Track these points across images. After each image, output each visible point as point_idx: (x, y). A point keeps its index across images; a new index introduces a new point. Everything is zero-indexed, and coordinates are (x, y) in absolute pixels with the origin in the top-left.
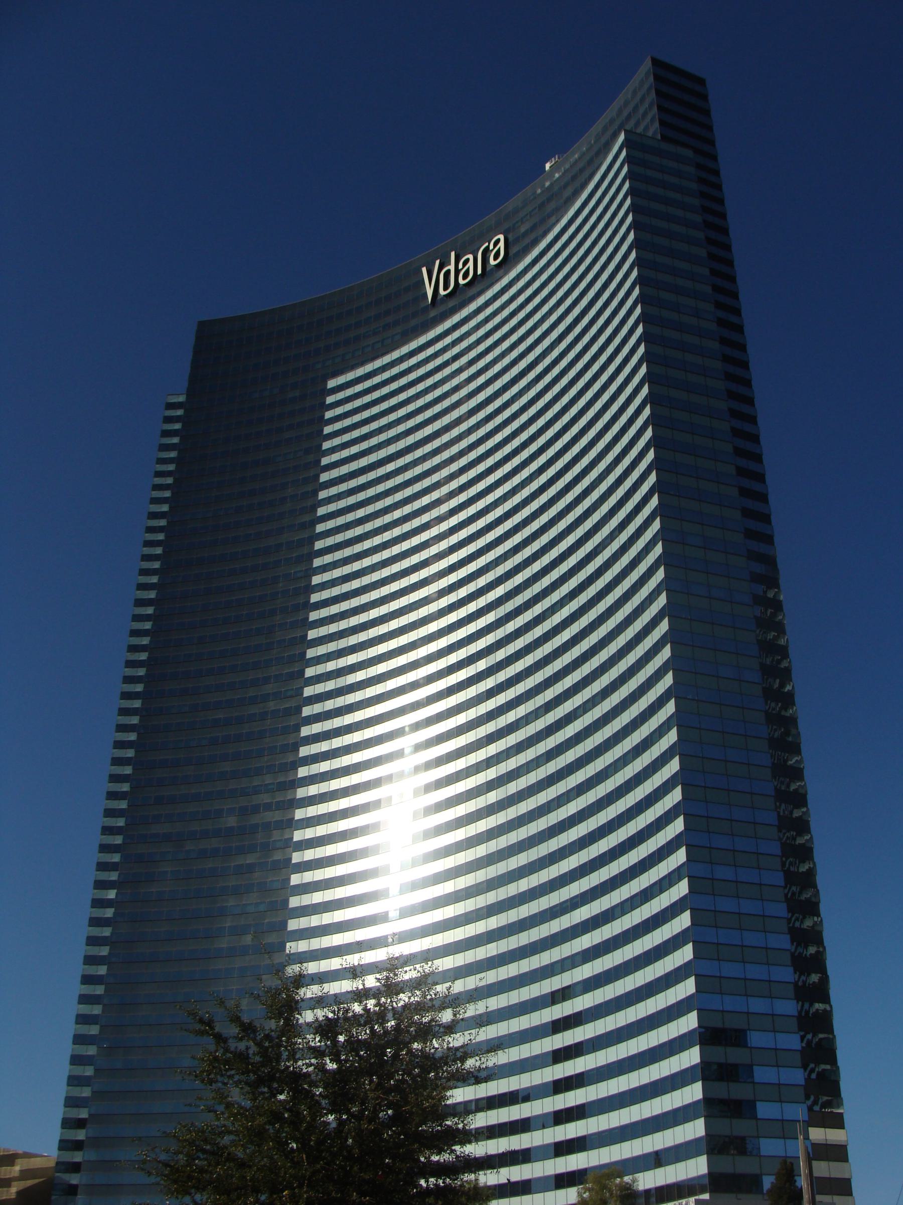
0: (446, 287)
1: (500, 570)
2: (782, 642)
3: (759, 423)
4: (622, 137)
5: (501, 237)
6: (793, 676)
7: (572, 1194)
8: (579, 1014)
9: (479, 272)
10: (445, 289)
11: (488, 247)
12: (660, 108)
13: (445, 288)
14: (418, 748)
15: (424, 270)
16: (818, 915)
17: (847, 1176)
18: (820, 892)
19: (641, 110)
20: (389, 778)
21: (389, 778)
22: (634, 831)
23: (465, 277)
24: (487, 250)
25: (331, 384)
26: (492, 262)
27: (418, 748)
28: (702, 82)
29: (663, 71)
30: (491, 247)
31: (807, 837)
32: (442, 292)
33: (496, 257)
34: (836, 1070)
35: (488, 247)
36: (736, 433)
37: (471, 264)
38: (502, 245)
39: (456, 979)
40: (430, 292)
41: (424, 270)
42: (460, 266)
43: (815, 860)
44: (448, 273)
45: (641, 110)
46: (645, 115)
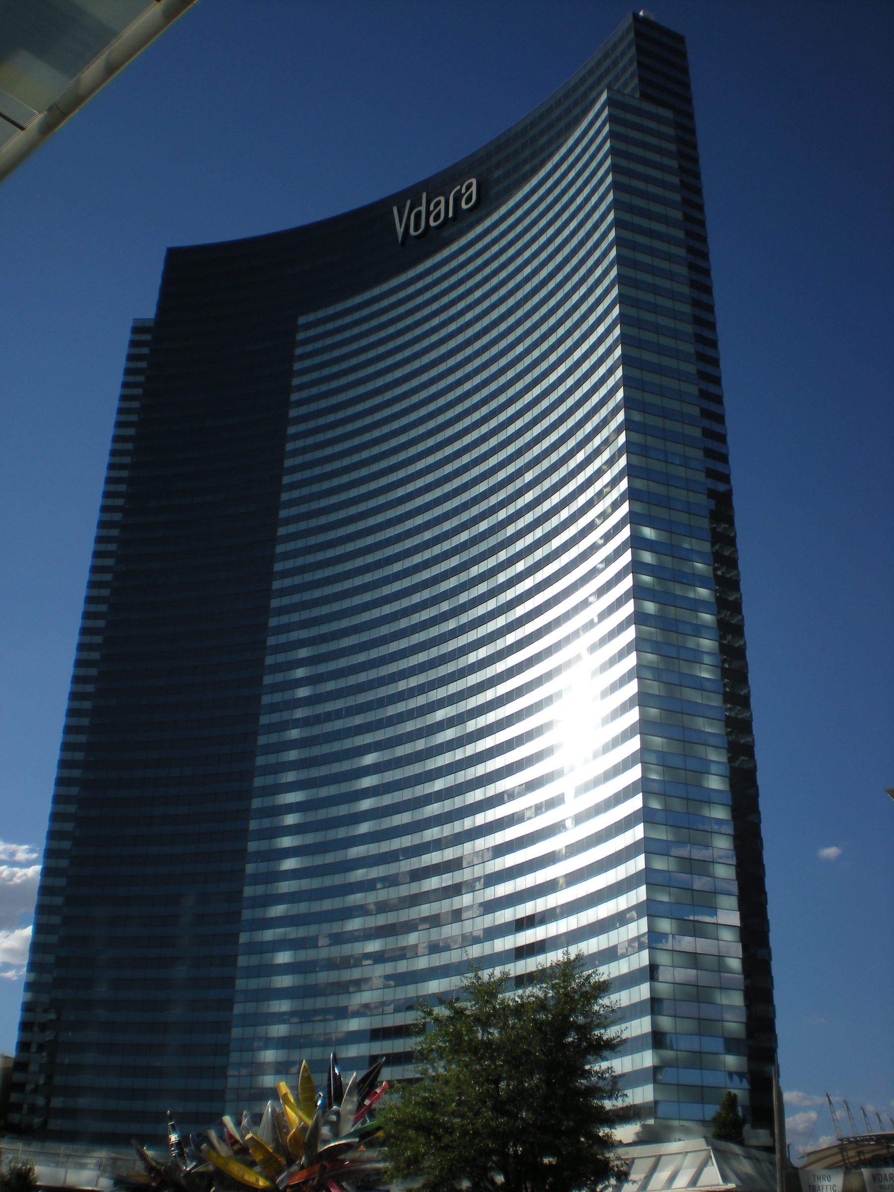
0: (416, 228)
4: (604, 96)
5: (474, 181)
8: (553, 909)
9: (451, 215)
11: (461, 189)
12: (641, 79)
13: (416, 229)
14: (593, 648)
15: (395, 209)
16: (735, 546)
18: (773, 951)
19: (621, 65)
20: (568, 664)
21: (568, 664)
23: (436, 219)
25: (302, 320)
26: (464, 206)
27: (593, 648)
28: (681, 39)
29: (644, 30)
30: (463, 191)
32: (412, 232)
33: (468, 200)
34: (746, 665)
37: (442, 206)
38: (474, 189)
40: (400, 230)
41: (395, 209)
42: (432, 208)
43: (744, 613)
44: (418, 214)
45: (621, 65)
46: (624, 70)
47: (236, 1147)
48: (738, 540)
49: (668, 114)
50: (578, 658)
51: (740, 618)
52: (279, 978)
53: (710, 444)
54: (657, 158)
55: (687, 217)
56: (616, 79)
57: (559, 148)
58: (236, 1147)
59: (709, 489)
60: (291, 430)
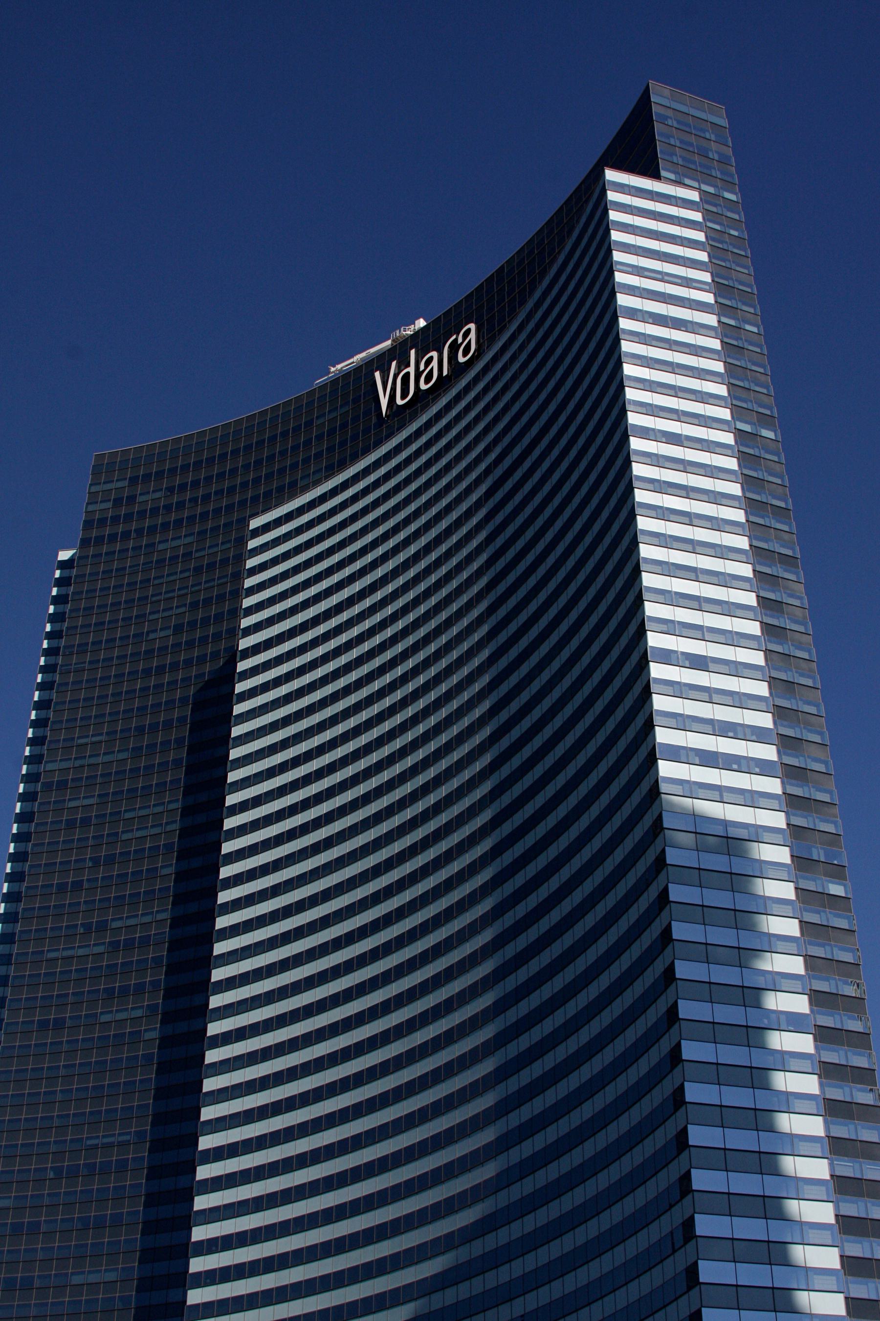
1: (362, 789)
5: (472, 326)
7: (407, 1310)
10: (403, 398)
11: (456, 340)
13: (403, 397)
15: (377, 375)
23: (427, 381)
26: (461, 359)
30: (460, 340)
32: (399, 402)
35: (456, 340)
37: (435, 364)
38: (473, 336)
39: (645, 1205)
40: (384, 402)
42: (422, 367)
60: (227, 847)
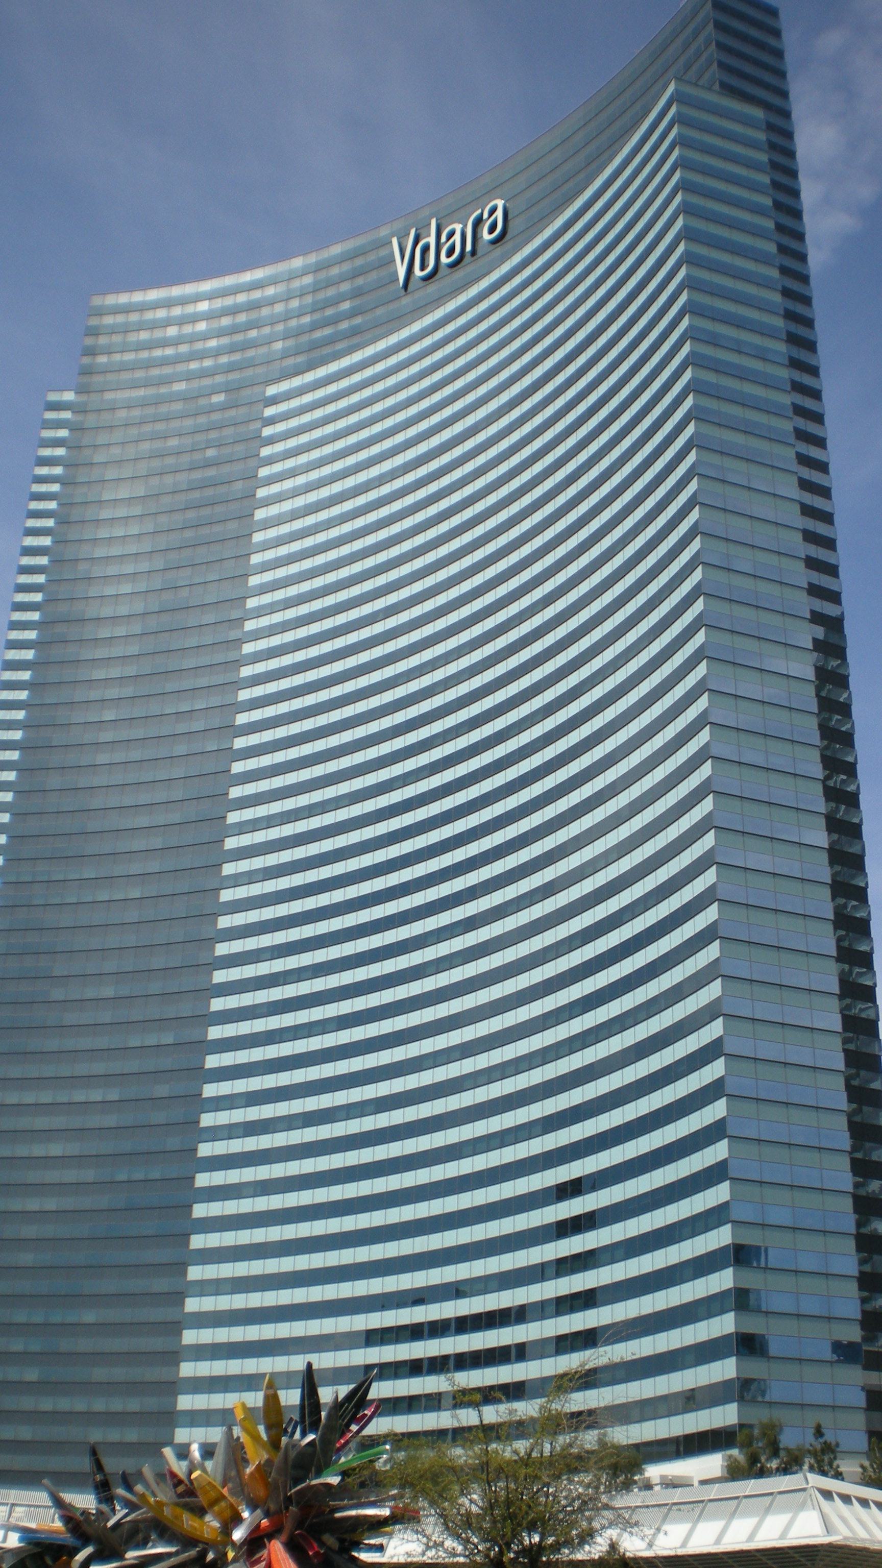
2: (852, 788)
3: (828, 446)
5: (500, 203)
6: (858, 772)
9: (469, 247)
11: (482, 214)
17: (833, 537)
22: (633, 1117)
24: (479, 222)
26: (486, 236)
28: (773, 12)
30: (485, 216)
31: (849, 726)
33: (492, 229)
36: (799, 411)
37: (457, 238)
38: (499, 214)
41: (395, 241)
42: (443, 239)
43: (851, 689)
44: (426, 249)
47: (181, 1489)
48: (865, 829)
49: (758, 113)
50: (703, 1482)
51: (849, 726)
52: (211, 1029)
53: (810, 499)
54: (746, 216)
55: (778, 206)
56: (688, 67)
57: (611, 159)
58: (181, 1489)
59: (810, 584)
